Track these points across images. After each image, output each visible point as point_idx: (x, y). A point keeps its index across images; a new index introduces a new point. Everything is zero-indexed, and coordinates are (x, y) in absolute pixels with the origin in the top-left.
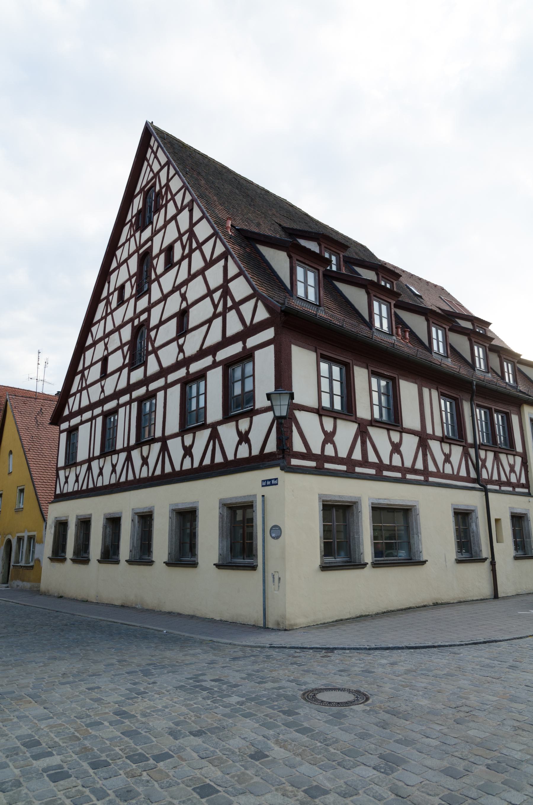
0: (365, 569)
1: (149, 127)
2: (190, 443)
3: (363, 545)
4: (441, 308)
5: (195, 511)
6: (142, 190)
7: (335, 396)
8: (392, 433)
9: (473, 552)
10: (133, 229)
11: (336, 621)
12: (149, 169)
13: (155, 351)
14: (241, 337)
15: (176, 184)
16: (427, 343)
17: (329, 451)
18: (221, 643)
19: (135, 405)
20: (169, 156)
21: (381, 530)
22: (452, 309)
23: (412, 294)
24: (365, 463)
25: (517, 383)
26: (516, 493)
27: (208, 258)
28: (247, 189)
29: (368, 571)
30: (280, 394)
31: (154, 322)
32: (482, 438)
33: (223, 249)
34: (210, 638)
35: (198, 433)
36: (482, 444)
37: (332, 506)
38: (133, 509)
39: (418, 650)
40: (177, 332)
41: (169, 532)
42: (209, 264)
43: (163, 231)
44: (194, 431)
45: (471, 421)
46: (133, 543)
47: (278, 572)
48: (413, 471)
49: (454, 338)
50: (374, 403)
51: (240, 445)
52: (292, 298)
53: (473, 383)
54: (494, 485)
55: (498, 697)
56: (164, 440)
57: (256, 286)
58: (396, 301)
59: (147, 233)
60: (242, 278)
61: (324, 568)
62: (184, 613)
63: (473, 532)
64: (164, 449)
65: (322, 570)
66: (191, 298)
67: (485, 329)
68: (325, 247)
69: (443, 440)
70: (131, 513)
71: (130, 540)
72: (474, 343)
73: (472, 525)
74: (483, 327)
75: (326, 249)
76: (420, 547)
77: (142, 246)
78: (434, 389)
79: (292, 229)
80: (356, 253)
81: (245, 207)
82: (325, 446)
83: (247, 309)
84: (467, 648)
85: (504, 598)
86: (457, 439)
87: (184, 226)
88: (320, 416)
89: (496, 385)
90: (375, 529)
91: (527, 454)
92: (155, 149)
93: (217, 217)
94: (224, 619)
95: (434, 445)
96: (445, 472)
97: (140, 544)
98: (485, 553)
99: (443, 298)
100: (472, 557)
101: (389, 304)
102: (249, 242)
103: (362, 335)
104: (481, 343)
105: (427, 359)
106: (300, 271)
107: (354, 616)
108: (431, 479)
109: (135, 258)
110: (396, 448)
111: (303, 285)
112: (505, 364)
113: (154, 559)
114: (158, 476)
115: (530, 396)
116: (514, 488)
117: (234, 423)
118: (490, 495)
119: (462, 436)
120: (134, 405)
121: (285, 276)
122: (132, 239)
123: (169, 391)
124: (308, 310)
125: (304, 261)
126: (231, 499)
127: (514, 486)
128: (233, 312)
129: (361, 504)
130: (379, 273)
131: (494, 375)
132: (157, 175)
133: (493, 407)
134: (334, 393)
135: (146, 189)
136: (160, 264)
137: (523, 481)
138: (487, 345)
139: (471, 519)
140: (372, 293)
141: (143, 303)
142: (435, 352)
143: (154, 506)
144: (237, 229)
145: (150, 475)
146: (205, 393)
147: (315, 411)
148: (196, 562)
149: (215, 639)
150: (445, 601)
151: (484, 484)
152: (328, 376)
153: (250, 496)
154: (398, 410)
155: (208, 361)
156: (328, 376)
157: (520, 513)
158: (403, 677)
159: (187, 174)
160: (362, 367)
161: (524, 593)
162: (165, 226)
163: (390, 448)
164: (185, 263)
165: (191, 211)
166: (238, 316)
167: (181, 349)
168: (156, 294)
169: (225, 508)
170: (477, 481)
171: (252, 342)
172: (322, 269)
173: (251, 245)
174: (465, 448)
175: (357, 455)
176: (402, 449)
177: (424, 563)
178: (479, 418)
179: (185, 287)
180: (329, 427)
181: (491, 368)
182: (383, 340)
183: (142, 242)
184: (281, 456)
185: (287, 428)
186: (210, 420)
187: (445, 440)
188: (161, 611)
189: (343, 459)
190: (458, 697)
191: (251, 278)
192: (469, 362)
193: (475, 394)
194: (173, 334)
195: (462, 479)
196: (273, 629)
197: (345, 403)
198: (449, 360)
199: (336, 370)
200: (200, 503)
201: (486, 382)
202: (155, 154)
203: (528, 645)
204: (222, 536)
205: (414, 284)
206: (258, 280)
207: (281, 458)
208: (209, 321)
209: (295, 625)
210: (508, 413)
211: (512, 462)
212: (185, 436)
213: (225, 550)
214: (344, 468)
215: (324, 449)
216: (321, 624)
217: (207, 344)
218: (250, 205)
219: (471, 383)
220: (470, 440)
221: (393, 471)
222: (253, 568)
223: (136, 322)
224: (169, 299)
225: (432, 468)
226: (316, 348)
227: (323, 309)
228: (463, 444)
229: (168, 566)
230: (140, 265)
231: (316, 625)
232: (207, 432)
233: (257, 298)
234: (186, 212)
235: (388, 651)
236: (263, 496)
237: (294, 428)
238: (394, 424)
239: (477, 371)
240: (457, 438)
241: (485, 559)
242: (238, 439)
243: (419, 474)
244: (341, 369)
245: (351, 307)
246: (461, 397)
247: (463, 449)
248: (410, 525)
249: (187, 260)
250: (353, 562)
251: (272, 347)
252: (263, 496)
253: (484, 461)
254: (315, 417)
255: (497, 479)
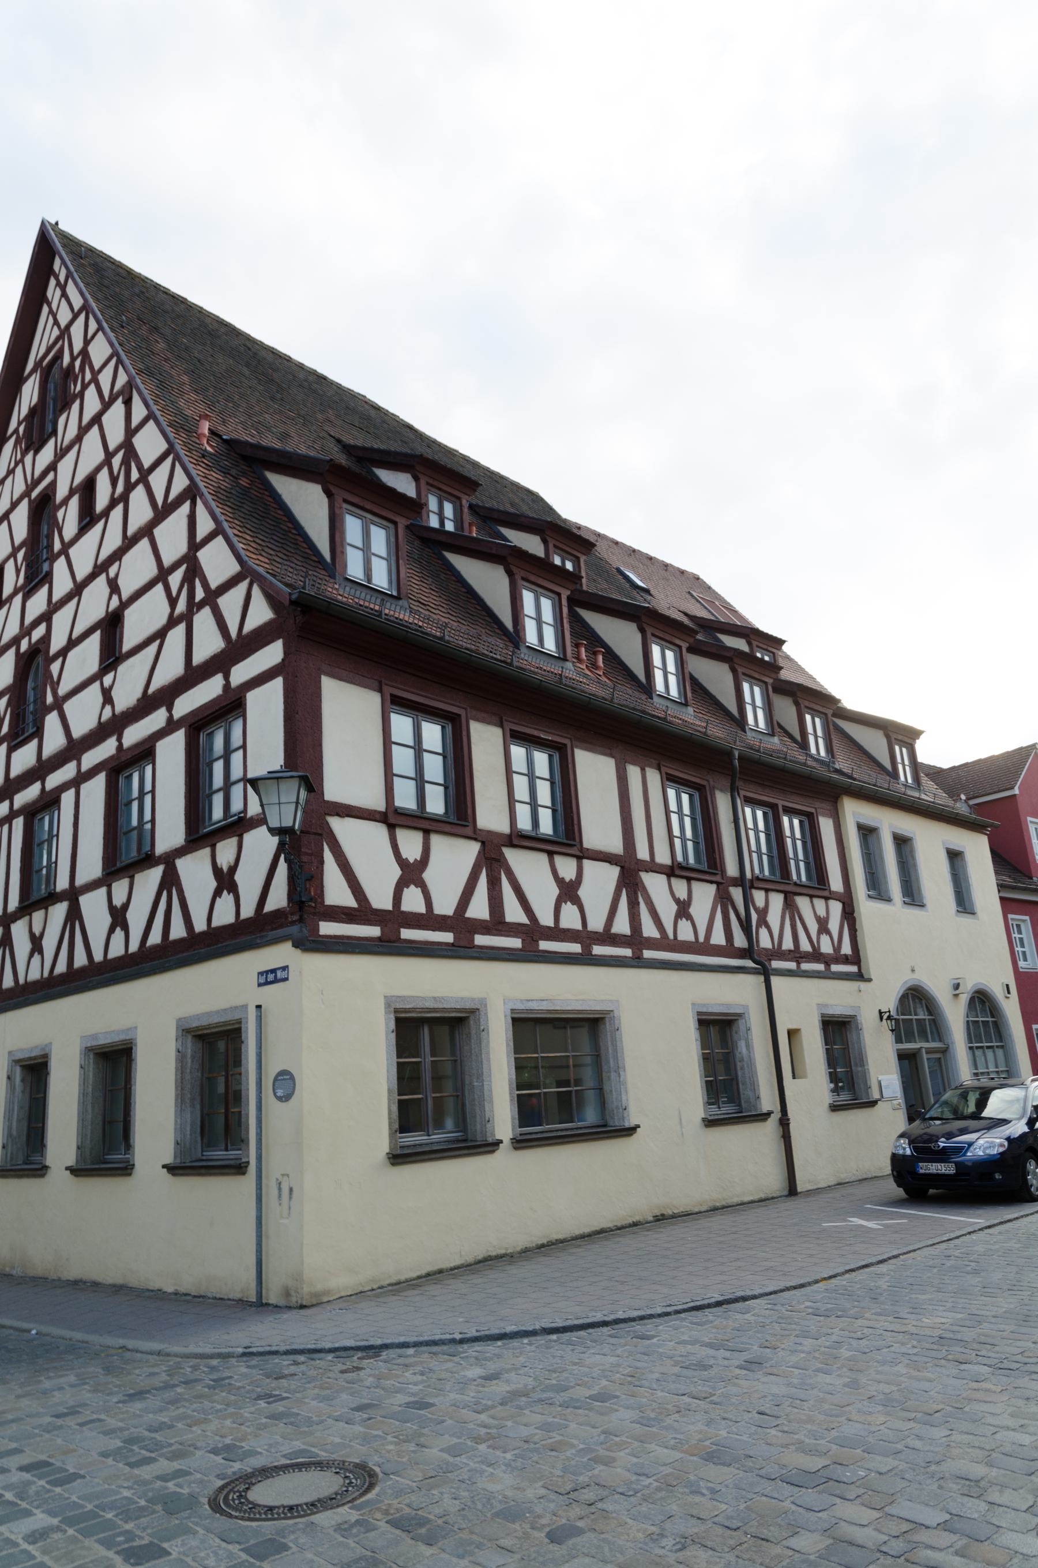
0: (497, 1154)
1: (48, 232)
2: (124, 899)
3: (491, 1102)
4: (689, 613)
5: (131, 1048)
6: (38, 364)
7: (427, 786)
8: (559, 860)
9: (743, 1102)
10: (21, 448)
11: (428, 1275)
12: (51, 320)
13: (58, 705)
14: (221, 663)
15: (100, 350)
16: (642, 678)
17: (413, 901)
18: (142, 1352)
19: (19, 823)
20: (84, 289)
21: (537, 1068)
22: (713, 615)
23: (627, 585)
24: (497, 924)
25: (833, 756)
26: (801, 974)
27: (160, 501)
28: (274, 370)
29: (504, 1159)
30: (277, 778)
31: (57, 642)
32: (759, 865)
33: (187, 482)
34: (121, 1342)
35: (138, 877)
36: (758, 879)
37: (420, 1022)
38: (10, 1053)
39: (566, 1336)
40: (102, 660)
41: (79, 1100)
42: (162, 513)
43: (76, 448)
44: (131, 874)
45: (734, 831)
46: (10, 1128)
47: (288, 1175)
48: (608, 937)
49: (705, 669)
50: (517, 798)
51: (218, 898)
52: (332, 580)
53: (734, 755)
54: (786, 960)
55: (682, 1452)
56: (73, 895)
57: (242, 553)
58: (572, 592)
59: (47, 454)
60: (220, 540)
61: (398, 1158)
62: (104, 1282)
63: (742, 1060)
64: (74, 915)
65: (393, 1164)
66: (127, 588)
67: (774, 653)
68: (428, 484)
69: (672, 871)
70: (6, 1062)
71: (4, 1122)
72: (741, 677)
73: (739, 1044)
74: (770, 649)
75: (430, 488)
76: (624, 1098)
77: (36, 482)
78: (650, 766)
79: (364, 449)
80: (512, 505)
81: (258, 401)
82: (402, 891)
83: (230, 603)
84: (674, 1321)
85: (809, 1193)
86: (706, 869)
87: (116, 436)
88: (392, 827)
89: (785, 759)
90: (520, 1067)
91: (853, 895)
92: (62, 278)
93: (180, 412)
94: (182, 1290)
95: (655, 884)
96: (679, 938)
97: (25, 1129)
98: (768, 1101)
99: (695, 594)
100: (741, 1112)
101: (557, 598)
102: (250, 467)
103: (492, 658)
104: (757, 676)
105: (637, 707)
106: (353, 527)
107: (470, 1259)
108: (648, 954)
109: (23, 509)
110: (569, 892)
111: (360, 554)
112: (897, 748)
113: (48, 1163)
114: (61, 975)
115: (855, 779)
116: (827, 965)
117: (207, 851)
118: (775, 980)
119: (715, 863)
120: (17, 822)
121: (319, 533)
122: (19, 470)
123: (85, 788)
124: (367, 604)
125: (361, 504)
126: (198, 1017)
127: (828, 961)
128: (207, 611)
129: (486, 1014)
130: (549, 539)
131: (786, 739)
132: (65, 332)
133: (780, 803)
134: (426, 778)
135: (45, 363)
136: (69, 518)
137: (846, 949)
138: (770, 681)
139: (736, 1033)
140: (519, 574)
141: (38, 604)
142: (659, 695)
143: (51, 1043)
144: (225, 441)
145: (46, 974)
146: (153, 792)
147: (378, 817)
148: (131, 1163)
149: (131, 1343)
150: (682, 1209)
151: (763, 959)
152: (411, 744)
153: (236, 1007)
154: (572, 812)
155: (157, 719)
156: (411, 744)
157: (841, 1016)
158: (492, 1412)
159: (123, 327)
160: (489, 723)
161: (853, 1178)
162: (79, 439)
163: (554, 891)
164: (117, 513)
165: (128, 403)
166: (216, 620)
167: (107, 697)
168: (62, 584)
169: (190, 1038)
170: (746, 953)
171: (241, 672)
172: (402, 523)
173: (254, 472)
174: (721, 887)
175: (479, 909)
176: (582, 892)
177: (632, 1130)
178: (750, 825)
179: (117, 564)
180: (682, 894)
181: (780, 726)
182: (541, 669)
183: (37, 473)
184: (296, 918)
185: (311, 855)
186: (162, 847)
187: (678, 872)
188: (59, 1280)
189: (444, 918)
190: (589, 1459)
191: (236, 535)
192: (733, 715)
193: (738, 775)
194: (93, 665)
195: (717, 951)
196: (276, 1306)
197: (451, 799)
198: (690, 710)
199: (541, 759)
200: (139, 1031)
201: (764, 753)
202: (64, 289)
203: (808, 1304)
204: (183, 1102)
205: (637, 568)
206: (254, 542)
207: (296, 921)
208: (161, 635)
209: (327, 1292)
210: (812, 813)
211: (821, 912)
212: (114, 885)
213: (188, 1133)
214: (447, 937)
215: (400, 898)
216: (390, 1285)
217: (155, 685)
218: (272, 398)
219: (728, 754)
220: (732, 870)
221: (562, 941)
222: (239, 1168)
223: (24, 645)
224: (86, 592)
225: (649, 930)
226: (380, 682)
227: (406, 605)
228: (718, 878)
229: (76, 1176)
230: (32, 524)
231: (379, 1288)
232: (154, 875)
233: (251, 580)
234: (118, 407)
235: (499, 1343)
236: (259, 1007)
237: (328, 856)
238: (565, 841)
239: (749, 733)
240: (704, 867)
241: (768, 1114)
242: (213, 884)
243: (622, 943)
244: (550, 757)
245: (478, 604)
246: (712, 783)
247: (718, 888)
248: (603, 1052)
249: (120, 507)
250: (471, 1141)
251: (278, 683)
252: (259, 1007)
253: (763, 913)
254: (380, 831)
255: (792, 947)
